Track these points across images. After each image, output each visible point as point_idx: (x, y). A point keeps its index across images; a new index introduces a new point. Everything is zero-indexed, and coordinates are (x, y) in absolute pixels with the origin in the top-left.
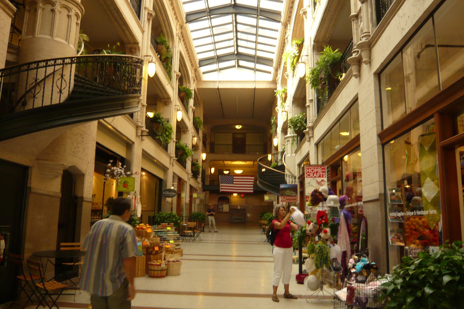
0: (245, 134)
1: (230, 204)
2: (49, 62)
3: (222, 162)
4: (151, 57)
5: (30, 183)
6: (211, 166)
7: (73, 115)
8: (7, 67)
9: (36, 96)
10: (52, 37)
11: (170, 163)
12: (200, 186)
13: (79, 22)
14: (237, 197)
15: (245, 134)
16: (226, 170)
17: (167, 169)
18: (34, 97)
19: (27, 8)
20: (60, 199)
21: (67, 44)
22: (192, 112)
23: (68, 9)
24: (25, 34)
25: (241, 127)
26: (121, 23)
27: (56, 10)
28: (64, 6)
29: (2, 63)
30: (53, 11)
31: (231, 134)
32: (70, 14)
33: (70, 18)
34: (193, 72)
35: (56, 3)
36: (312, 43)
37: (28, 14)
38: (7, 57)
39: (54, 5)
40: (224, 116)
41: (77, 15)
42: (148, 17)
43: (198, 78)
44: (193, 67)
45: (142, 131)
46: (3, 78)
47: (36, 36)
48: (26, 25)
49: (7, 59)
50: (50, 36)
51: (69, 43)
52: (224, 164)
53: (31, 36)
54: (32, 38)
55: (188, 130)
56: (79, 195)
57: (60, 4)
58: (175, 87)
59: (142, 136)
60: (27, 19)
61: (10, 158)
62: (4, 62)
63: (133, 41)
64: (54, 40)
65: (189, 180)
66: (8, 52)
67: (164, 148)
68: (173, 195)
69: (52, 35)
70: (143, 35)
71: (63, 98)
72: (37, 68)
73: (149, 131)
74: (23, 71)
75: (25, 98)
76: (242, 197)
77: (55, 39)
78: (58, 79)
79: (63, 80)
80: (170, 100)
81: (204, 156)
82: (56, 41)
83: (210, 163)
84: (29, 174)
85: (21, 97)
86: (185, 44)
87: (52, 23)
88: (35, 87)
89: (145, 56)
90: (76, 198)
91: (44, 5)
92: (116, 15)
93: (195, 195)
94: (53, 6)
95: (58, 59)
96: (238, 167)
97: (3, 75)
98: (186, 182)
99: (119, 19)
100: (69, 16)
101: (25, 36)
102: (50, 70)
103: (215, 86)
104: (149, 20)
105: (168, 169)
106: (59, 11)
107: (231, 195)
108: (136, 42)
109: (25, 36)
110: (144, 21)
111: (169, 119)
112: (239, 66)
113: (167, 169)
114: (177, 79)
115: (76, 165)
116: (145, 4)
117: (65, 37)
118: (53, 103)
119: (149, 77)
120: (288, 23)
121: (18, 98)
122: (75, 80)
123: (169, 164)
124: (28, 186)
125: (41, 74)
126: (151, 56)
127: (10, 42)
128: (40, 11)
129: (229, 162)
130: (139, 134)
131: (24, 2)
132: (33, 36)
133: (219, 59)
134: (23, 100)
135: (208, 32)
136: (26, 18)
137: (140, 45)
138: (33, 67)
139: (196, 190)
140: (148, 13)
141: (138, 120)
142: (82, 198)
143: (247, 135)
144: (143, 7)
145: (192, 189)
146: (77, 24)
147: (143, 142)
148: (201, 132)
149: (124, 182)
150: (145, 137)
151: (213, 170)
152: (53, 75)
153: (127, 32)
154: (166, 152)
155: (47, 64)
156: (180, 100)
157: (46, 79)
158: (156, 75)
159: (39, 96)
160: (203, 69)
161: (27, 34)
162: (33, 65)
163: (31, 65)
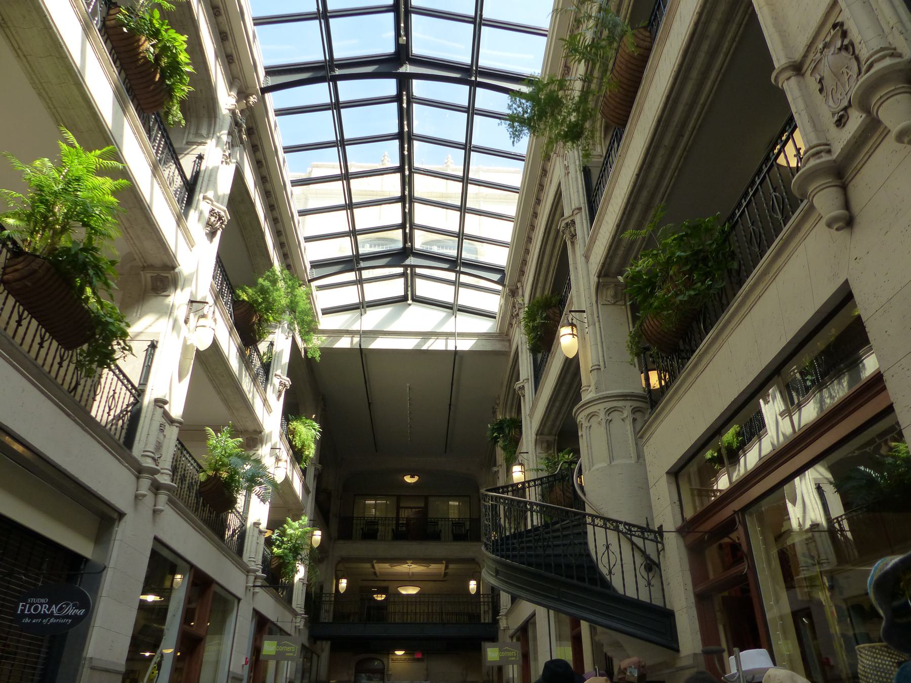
3: (368, 565)
6: (339, 573)
12: (300, 623)
14: (405, 660)
16: (380, 592)
25: (416, 479)
36: (534, 436)
52: (375, 574)
65: (254, 594)
68: (67, 617)
76: (418, 660)
93: (269, 647)
96: (410, 580)
98: (239, 600)
107: (388, 654)
119: (197, 350)
120: (519, 285)
126: (207, 303)
141: (251, 559)
145: (262, 625)
151: (343, 583)
158: (215, 345)
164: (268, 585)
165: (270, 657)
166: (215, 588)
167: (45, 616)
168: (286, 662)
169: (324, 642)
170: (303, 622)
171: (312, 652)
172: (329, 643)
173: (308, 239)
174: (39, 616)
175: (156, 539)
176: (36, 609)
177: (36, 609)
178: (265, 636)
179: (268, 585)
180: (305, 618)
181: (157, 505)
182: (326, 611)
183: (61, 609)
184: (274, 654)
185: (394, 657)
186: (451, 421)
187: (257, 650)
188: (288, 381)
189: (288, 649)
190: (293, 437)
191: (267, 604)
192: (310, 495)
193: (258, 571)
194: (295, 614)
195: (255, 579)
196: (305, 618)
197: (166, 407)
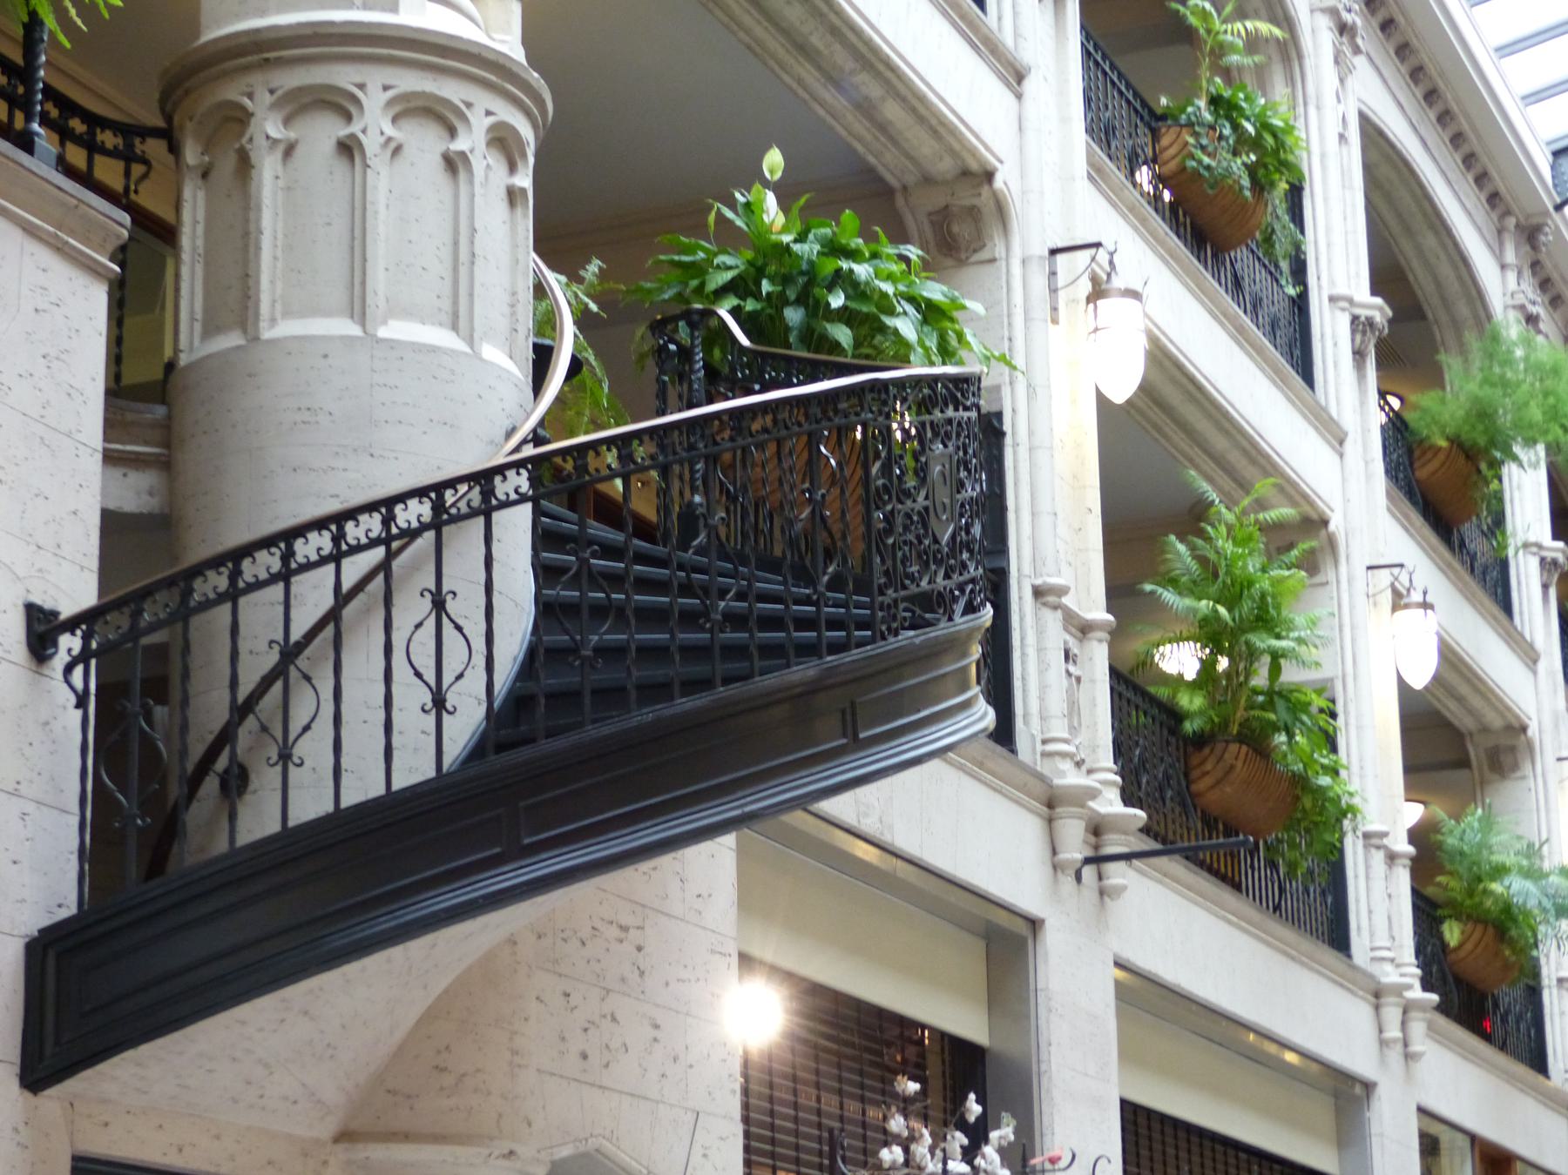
2: (350, 526)
4: (1102, 256)
7: (527, 841)
8: (112, 597)
9: (299, 750)
10: (363, 324)
11: (1383, 1043)
13: (524, 180)
18: (285, 757)
19: (192, 154)
21: (460, 345)
22: (1545, 587)
23: (445, 118)
24: (198, 327)
27: (371, 143)
28: (420, 103)
29: (82, 568)
30: (348, 149)
32: (460, 144)
33: (462, 175)
34: (1510, 256)
37: (201, 195)
38: (105, 492)
39: (353, 109)
41: (502, 140)
44: (1508, 212)
45: (1097, 829)
46: (93, 662)
47: (267, 334)
51: (470, 341)
54: (239, 348)
55: (1530, 746)
57: (390, 94)
58: (1539, 644)
59: (1097, 860)
62: (95, 521)
63: (945, 167)
64: (380, 341)
66: (109, 458)
67: (1314, 933)
69: (364, 314)
73: (1150, 817)
74: (207, 605)
75: (233, 755)
77: (383, 333)
78: (419, 626)
79: (430, 677)
82: (392, 344)
85: (210, 738)
86: (1403, 51)
87: (352, 230)
91: (287, 122)
94: (348, 118)
95: (402, 498)
97: (94, 645)
100: (454, 164)
101: (197, 342)
105: (1369, 1087)
106: (389, 139)
113: (1358, 1090)
114: (1359, 354)
115: (608, 1147)
117: (446, 304)
118: (398, 783)
121: (197, 751)
122: (545, 573)
123: (1375, 1046)
127: (113, 385)
128: (268, 169)
130: (1075, 847)
131: (169, 119)
134: (222, 763)
136: (196, 222)
138: (263, 575)
141: (1051, 747)
146: (513, 195)
147: (1119, 909)
150: (1120, 866)
152: (380, 578)
154: (1330, 956)
155: (338, 539)
156: (1417, 519)
157: (348, 612)
158: (1162, 359)
159: (314, 749)
161: (211, 328)
162: (262, 556)
163: (246, 564)
173: (1505, 50)
175: (1422, 1111)
181: (1058, 849)
188: (1381, 309)
193: (1409, 987)
195: (1405, 1012)
197: (1066, 600)
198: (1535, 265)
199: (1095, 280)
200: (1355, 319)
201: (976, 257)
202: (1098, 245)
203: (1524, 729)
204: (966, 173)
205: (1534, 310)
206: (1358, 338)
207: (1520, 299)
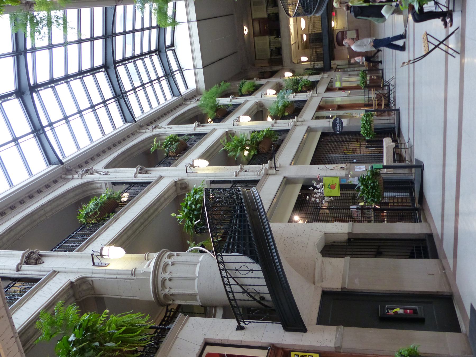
0: (253, 20)
1: (346, 30)
5: (338, 289)
10: (196, 278)
12: (325, 75)
15: (253, 20)
17: (309, 129)
19: (171, 302)
20: (345, 327)
22: (236, 99)
23: (166, 265)
24: (196, 302)
26: (158, 204)
27: (170, 276)
30: (170, 280)
31: (256, 38)
32: (170, 263)
34: (144, 131)
35: (162, 278)
39: (165, 279)
40: (235, 53)
41: (169, 257)
42: (143, 173)
43: (195, 94)
46: (245, 320)
48: (187, 302)
49: (221, 317)
50: (195, 280)
51: (199, 262)
52: (295, 43)
53: (198, 297)
56: (346, 237)
58: (245, 100)
60: (181, 301)
61: (316, 308)
65: (319, 94)
69: (194, 278)
70: (59, 272)
71: (257, 267)
72: (232, 292)
76: (336, 14)
80: (228, 132)
81: (288, 74)
83: (294, 63)
84: (329, 290)
88: (249, 293)
89: (94, 263)
90: (349, 239)
91: (166, 288)
92: (152, 211)
93: (338, 85)
94: (166, 279)
96: (297, 25)
98: (331, 79)
99: (156, 207)
100: (173, 264)
101: (198, 302)
102: (232, 281)
103: (201, 72)
104: (146, 172)
107: (334, 30)
108: (174, 184)
109: (198, 302)
110: (149, 177)
111: (250, 131)
112: (172, 45)
113: (309, 129)
116: (131, 177)
124: (340, 290)
125: (237, 288)
129: (292, 37)
130: (273, 171)
132: (197, 295)
133: (169, 74)
135: (141, 93)
136: (181, 302)
137: (73, 278)
138: (232, 296)
139: (331, 82)
140: (139, 173)
142: (349, 234)
143: (254, 17)
144: (134, 180)
145: (330, 89)
146: (177, 255)
148: (258, 82)
149: (330, 188)
151: (304, 59)
153: (166, 196)
156: (227, 118)
159: (258, 288)
160: (183, 90)
164: (273, 159)
165: (341, 84)
166: (329, 87)
167: (339, 127)
168: (343, 79)
169: (332, 64)
170: (325, 75)
171: (336, 69)
172: (332, 61)
174: (339, 128)
176: (338, 129)
177: (338, 129)
178: (334, 87)
179: (273, 159)
180: (323, 74)
182: (317, 65)
183: (338, 124)
184: (340, 82)
185: (335, 27)
186: (250, 5)
187: (341, 89)
188: (196, 123)
189: (338, 77)
190: (250, 91)
191: (321, 89)
192: (269, 81)
193: (294, 121)
194: (322, 78)
195: (298, 121)
196: (323, 74)
198: (190, 99)
199: (191, 166)
200: (197, 127)
201: (187, 183)
202: (186, 166)
203: (257, 102)
204: (257, 104)
205: (196, 100)
206: (200, 126)
207: (151, 130)
